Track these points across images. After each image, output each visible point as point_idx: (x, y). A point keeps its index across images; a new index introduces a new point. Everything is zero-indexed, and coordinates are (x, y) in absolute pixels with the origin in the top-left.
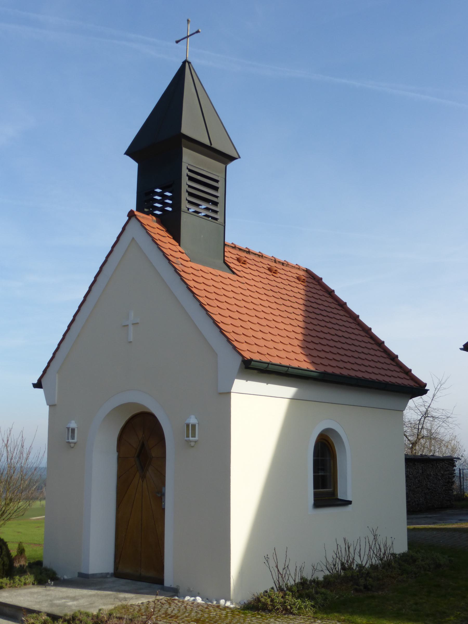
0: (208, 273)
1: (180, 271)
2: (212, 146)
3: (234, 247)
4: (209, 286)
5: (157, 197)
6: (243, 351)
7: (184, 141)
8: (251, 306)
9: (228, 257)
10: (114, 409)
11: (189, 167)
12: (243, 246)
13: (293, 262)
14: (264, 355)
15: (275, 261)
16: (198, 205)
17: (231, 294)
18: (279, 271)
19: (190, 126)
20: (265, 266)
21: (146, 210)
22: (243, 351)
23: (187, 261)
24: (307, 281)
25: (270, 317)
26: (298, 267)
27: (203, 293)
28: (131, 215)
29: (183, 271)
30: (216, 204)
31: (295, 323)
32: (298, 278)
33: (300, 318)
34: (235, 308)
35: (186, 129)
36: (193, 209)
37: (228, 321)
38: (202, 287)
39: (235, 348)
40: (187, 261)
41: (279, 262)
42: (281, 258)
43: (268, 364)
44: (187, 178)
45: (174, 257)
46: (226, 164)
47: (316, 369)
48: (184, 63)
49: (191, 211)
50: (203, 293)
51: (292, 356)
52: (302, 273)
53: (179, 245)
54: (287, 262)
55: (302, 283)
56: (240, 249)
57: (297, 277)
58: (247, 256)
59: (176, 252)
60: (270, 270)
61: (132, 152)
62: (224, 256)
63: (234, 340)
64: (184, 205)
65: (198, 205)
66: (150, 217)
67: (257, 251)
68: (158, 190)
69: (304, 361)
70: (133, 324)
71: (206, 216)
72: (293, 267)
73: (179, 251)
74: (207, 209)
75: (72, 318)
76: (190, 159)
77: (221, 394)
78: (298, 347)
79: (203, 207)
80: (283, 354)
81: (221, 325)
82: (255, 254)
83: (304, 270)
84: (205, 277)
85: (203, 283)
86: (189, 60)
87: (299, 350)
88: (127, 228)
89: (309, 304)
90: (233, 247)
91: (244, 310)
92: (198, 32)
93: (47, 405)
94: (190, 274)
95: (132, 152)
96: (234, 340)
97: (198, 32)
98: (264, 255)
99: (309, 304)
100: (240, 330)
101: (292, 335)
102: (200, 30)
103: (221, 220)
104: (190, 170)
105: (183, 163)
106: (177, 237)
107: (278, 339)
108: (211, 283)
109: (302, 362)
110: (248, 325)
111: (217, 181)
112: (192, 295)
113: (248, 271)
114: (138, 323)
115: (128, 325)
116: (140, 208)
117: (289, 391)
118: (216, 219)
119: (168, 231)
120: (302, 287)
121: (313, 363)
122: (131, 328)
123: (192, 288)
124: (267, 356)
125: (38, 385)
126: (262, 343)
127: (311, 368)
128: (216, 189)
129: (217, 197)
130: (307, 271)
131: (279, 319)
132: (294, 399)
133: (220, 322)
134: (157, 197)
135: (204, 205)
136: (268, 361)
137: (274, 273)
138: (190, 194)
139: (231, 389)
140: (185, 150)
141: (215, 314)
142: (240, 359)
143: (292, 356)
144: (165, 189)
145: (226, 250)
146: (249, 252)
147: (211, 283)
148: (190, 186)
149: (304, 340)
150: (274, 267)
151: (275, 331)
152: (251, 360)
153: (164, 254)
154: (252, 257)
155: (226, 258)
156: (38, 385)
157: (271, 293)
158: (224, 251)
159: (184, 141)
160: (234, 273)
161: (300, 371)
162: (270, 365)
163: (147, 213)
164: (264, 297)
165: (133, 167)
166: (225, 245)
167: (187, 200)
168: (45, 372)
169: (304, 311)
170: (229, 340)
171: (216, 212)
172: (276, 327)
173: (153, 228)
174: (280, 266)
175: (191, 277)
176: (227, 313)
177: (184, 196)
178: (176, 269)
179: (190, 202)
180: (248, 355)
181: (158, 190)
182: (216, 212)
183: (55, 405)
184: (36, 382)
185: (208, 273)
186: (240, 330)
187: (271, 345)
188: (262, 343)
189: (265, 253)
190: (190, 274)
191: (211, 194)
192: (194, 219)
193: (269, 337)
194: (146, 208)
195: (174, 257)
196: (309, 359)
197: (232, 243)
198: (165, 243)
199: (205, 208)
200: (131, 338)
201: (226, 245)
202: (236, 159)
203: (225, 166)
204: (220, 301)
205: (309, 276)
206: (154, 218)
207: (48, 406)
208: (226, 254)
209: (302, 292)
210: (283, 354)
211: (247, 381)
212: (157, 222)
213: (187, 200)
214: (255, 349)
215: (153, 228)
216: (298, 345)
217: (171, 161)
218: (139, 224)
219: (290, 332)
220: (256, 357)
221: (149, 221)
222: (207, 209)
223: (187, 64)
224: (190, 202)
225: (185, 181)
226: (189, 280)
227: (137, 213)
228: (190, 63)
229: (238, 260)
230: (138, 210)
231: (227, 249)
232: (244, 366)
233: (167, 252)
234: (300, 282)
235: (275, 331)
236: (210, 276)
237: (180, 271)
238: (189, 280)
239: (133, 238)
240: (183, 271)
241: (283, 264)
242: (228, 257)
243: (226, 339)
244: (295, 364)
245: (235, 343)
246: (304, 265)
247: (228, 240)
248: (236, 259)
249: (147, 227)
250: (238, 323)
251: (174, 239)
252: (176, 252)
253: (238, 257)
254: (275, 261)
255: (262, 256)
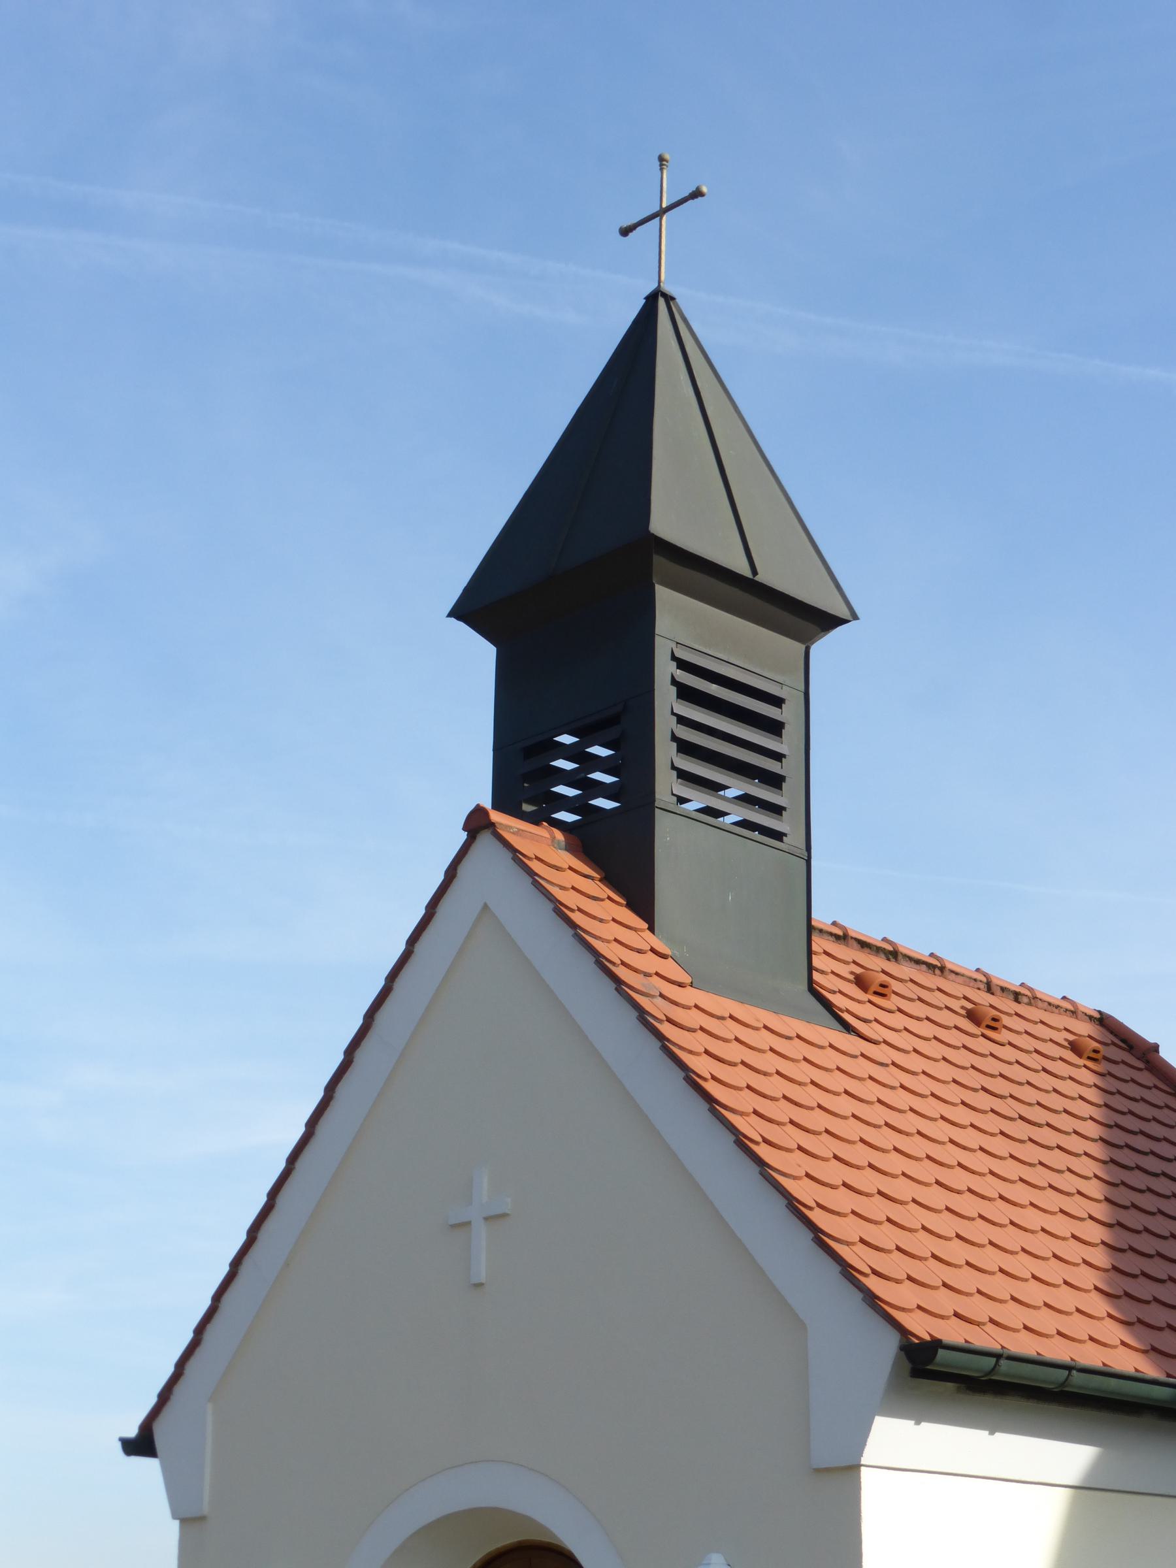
0: (757, 1029)
1: (660, 1021)
2: (758, 578)
3: (843, 938)
4: (765, 1074)
5: (562, 764)
6: (903, 1310)
7: (659, 562)
8: (918, 1147)
9: (822, 972)
10: (417, 1533)
11: (681, 654)
12: (875, 935)
13: (1051, 990)
14: (978, 1324)
15: (989, 988)
16: (715, 787)
17: (845, 1105)
18: (1006, 1020)
19: (680, 510)
20: (956, 1005)
21: (527, 808)
22: (903, 1310)
23: (681, 985)
24: (1105, 1058)
25: (990, 1187)
26: (1070, 1007)
27: (746, 1102)
28: (477, 823)
29: (670, 1020)
30: (775, 781)
31: (1076, 1206)
32: (1075, 1048)
33: (1095, 1189)
34: (860, 1155)
35: (665, 522)
36: (698, 800)
37: (842, 1200)
38: (740, 1076)
39: (872, 1300)
40: (681, 985)
41: (1003, 989)
42: (1011, 977)
43: (998, 1356)
44: (673, 690)
45: (636, 970)
46: (807, 640)
47: (1169, 1375)
48: (652, 300)
49: (690, 807)
50: (746, 1102)
51: (1079, 1327)
52: (1084, 1029)
53: (651, 929)
54: (1030, 989)
55: (1090, 1064)
56: (864, 945)
57: (1070, 1043)
58: (891, 967)
59: (639, 951)
60: (973, 1016)
61: (467, 610)
62: (811, 968)
63: (868, 1271)
64: (666, 785)
65: (715, 787)
66: (543, 831)
67: (922, 950)
68: (566, 739)
69: (1123, 1343)
70: (486, 1219)
71: (745, 824)
72: (1052, 1007)
73: (653, 950)
74: (746, 799)
75: (264, 1199)
76: (681, 624)
77: (818, 1471)
78: (1095, 1295)
79: (731, 793)
80: (1045, 1321)
81: (816, 1216)
82: (918, 962)
83: (1091, 1018)
84: (747, 1040)
85: (743, 1063)
86: (667, 288)
87: (1100, 1306)
88: (462, 870)
89: (1119, 1137)
90: (837, 937)
91: (894, 1163)
92: (697, 194)
93: (174, 1517)
94: (694, 1031)
95: (467, 610)
96: (868, 1271)
97: (697, 194)
98: (949, 966)
99: (1119, 1137)
100: (886, 1236)
101: (1073, 1251)
102: (704, 189)
103: (794, 839)
104: (683, 665)
105: (657, 639)
106: (642, 902)
107: (1022, 1265)
108: (769, 1062)
109: (1109, 1347)
110: (913, 1216)
111: (777, 702)
112: (703, 1106)
113: (898, 1020)
114: (504, 1216)
115: (469, 1223)
116: (505, 798)
117: (1066, 1458)
118: (778, 836)
119: (609, 880)
120: (1090, 1078)
121: (1154, 1351)
122: (481, 1233)
123: (705, 1080)
124: (990, 1328)
125: (141, 1445)
126: (966, 1280)
127: (1149, 1369)
128: (775, 728)
129: (778, 757)
130: (1103, 1020)
131: (1020, 1193)
132: (1087, 1488)
133: (813, 1204)
134: (562, 764)
135: (736, 787)
136: (996, 1347)
137: (988, 1027)
138: (686, 748)
139: (860, 1453)
140: (663, 594)
141: (795, 1178)
142: (890, 1343)
143: (1079, 1327)
144: (587, 734)
145: (815, 947)
146: (894, 954)
147: (769, 1062)
148: (682, 720)
149: (1115, 1268)
150: (989, 1007)
151: (1011, 1238)
152: (936, 1344)
153: (602, 963)
154: (904, 970)
155: (816, 976)
156: (141, 1445)
157: (983, 1101)
158: (810, 953)
159: (659, 562)
160: (848, 1028)
161: (1113, 1382)
162: (1003, 1362)
163: (534, 819)
164: (962, 1115)
165: (477, 658)
166: (810, 928)
167: (673, 767)
168: (165, 1396)
169: (1104, 1162)
170: (847, 1271)
171: (777, 810)
172: (1012, 1223)
173: (558, 869)
174: (1008, 1005)
175: (698, 1042)
176: (834, 1173)
177: (665, 753)
178: (642, 1015)
179: (685, 776)
180: (921, 1327)
181: (566, 739)
182: (777, 810)
183: (202, 1519)
184: (132, 1432)
185: (757, 1029)
186: (886, 1236)
187: (999, 1286)
188: (966, 1280)
189: (953, 958)
190: (694, 1031)
191: (756, 747)
192: (703, 835)
193: (990, 1259)
194: (529, 802)
195: (636, 970)
196: (1136, 1336)
197: (834, 924)
198: (601, 921)
199: (739, 798)
200: (481, 1272)
201: (814, 928)
202: (845, 621)
203: (803, 647)
204: (807, 1131)
205: (1109, 1038)
206: (559, 835)
207: (177, 1523)
208: (817, 961)
209: (1092, 1095)
210: (1045, 1321)
211: (918, 1423)
212: (569, 848)
213: (673, 767)
214: (945, 1302)
215: (558, 869)
216: (1096, 1288)
217: (609, 639)
218: (508, 855)
219: (1064, 1239)
220: (952, 1333)
221: (543, 844)
222: (746, 799)
223: (661, 302)
224: (683, 775)
225: (665, 700)
226: (691, 1052)
227: (496, 817)
228: (673, 299)
229: (861, 982)
230: (496, 805)
231: (819, 943)
232: (907, 1366)
233: (611, 952)
234: (1081, 1062)
235: (1011, 1238)
236: (764, 1040)
237: (660, 1021)
238: (691, 1052)
239: (486, 907)
240: (670, 1020)
241: (1017, 997)
242: (822, 972)
243: (838, 1268)
244: (1091, 1357)
245: (872, 1283)
246: (1091, 1002)
247: (822, 915)
248: (851, 977)
249: (535, 866)
250: (878, 1208)
251: (631, 906)
252: (639, 951)
253: (858, 970)
254: (989, 988)
255: (942, 969)
